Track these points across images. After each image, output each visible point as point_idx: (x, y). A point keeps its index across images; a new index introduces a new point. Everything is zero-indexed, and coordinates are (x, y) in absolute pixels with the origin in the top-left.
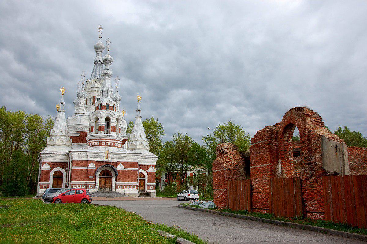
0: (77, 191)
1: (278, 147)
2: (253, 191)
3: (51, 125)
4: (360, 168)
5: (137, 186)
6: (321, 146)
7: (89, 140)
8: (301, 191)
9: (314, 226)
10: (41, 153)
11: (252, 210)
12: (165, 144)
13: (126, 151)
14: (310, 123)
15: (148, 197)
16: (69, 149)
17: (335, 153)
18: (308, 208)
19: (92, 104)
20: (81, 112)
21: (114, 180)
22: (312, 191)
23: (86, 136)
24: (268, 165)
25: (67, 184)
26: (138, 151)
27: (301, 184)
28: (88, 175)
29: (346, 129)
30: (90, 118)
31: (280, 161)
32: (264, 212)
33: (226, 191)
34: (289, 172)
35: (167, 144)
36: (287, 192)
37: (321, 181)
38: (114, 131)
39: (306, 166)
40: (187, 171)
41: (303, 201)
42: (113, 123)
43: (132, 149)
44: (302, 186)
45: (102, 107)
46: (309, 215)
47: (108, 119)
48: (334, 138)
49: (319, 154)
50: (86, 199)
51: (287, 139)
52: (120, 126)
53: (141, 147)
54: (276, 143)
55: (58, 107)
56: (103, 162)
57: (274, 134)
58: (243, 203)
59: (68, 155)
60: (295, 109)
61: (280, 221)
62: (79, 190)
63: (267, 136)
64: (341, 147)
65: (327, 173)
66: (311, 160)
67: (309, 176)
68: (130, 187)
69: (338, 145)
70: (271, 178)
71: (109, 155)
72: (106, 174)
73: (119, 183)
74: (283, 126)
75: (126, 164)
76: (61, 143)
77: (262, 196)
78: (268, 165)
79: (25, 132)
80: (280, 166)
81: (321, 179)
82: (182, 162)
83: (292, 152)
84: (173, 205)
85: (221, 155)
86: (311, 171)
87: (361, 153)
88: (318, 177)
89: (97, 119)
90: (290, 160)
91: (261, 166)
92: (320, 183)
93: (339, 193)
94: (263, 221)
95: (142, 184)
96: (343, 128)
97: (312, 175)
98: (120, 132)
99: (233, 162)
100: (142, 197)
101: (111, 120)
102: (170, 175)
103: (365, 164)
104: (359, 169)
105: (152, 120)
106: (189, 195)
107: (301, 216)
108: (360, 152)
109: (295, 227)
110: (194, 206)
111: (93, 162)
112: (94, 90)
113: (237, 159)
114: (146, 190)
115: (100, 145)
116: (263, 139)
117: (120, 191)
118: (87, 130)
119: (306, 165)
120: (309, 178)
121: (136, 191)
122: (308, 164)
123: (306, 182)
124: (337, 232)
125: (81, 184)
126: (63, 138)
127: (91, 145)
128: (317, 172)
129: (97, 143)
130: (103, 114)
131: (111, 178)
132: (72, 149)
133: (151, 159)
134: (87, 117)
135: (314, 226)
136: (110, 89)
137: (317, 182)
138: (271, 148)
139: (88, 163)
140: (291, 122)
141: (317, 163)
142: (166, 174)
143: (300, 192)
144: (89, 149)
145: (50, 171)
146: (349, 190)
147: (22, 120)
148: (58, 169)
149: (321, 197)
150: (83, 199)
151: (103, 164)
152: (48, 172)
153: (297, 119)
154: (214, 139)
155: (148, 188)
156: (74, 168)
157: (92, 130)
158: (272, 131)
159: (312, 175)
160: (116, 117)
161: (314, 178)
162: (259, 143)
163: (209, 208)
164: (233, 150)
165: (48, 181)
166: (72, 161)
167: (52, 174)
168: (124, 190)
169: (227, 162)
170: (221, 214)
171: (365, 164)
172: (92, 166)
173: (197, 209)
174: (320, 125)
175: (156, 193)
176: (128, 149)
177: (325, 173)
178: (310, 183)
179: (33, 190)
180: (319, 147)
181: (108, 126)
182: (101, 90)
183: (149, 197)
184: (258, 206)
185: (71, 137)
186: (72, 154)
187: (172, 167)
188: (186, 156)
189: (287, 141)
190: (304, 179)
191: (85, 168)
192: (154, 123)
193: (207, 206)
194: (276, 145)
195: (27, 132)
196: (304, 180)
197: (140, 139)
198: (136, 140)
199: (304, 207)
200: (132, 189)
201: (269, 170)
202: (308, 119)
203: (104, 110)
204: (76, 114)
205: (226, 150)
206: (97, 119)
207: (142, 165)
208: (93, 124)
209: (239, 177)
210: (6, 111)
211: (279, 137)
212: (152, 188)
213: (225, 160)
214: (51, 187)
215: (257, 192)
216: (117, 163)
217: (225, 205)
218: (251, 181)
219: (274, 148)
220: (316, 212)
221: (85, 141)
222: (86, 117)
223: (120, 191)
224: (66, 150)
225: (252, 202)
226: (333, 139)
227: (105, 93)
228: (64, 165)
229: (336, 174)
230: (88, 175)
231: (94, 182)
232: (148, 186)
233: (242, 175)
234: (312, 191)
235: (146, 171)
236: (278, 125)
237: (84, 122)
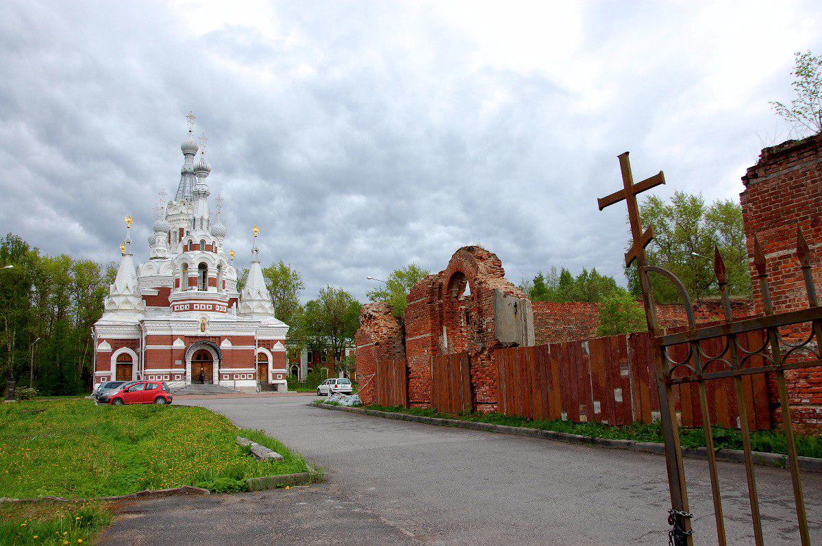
0: (147, 384)
2: (411, 375)
3: (112, 276)
5: (255, 374)
6: (494, 305)
7: (174, 301)
9: (480, 423)
10: (96, 324)
11: (409, 404)
12: (308, 305)
13: (235, 318)
14: (484, 270)
15: (274, 392)
16: (141, 317)
18: (479, 397)
19: (178, 241)
20: (160, 255)
21: (216, 365)
22: (483, 372)
23: (169, 295)
24: (429, 335)
25: (140, 375)
26: (256, 318)
27: (469, 359)
28: (171, 358)
29: (594, 273)
30: (173, 265)
31: (445, 328)
32: (425, 406)
33: (374, 377)
35: (310, 304)
38: (215, 285)
39: (475, 335)
40: (345, 347)
41: (472, 388)
42: (211, 274)
43: (245, 315)
44: (470, 365)
45: (193, 247)
46: (479, 408)
47: (203, 267)
48: (512, 293)
50: (163, 397)
52: (224, 277)
53: (260, 310)
55: (123, 247)
56: (196, 337)
58: (396, 395)
59: (140, 327)
60: (464, 248)
61: (439, 419)
62: (151, 383)
64: (522, 306)
68: (243, 377)
71: (207, 326)
72: (202, 358)
73: (223, 370)
74: (449, 275)
75: (235, 340)
76: (127, 307)
77: (421, 383)
78: (429, 335)
79: (72, 290)
82: (335, 333)
84: (302, 403)
87: (585, 311)
88: (491, 351)
89: (186, 266)
90: (462, 327)
91: (419, 337)
93: (514, 372)
94: (419, 421)
95: (264, 372)
96: (589, 272)
97: (484, 349)
98: (224, 288)
99: (385, 332)
100: (263, 393)
101: (209, 267)
102: (316, 357)
105: (282, 266)
106: (336, 386)
107: (469, 409)
109: (457, 425)
110: (332, 403)
111: (180, 336)
112: (182, 218)
113: (392, 328)
114: (271, 380)
115: (191, 309)
116: (421, 296)
117: (227, 383)
118: (170, 284)
120: (480, 353)
121: (253, 383)
122: (479, 332)
125: (163, 375)
126: (131, 299)
127: (176, 309)
129: (208, 306)
130: (195, 257)
131: (212, 362)
132: (145, 316)
133: (277, 330)
134: (170, 263)
135: (480, 423)
136: (206, 217)
137: (489, 357)
138: (432, 310)
139: (172, 339)
142: (309, 355)
144: (173, 317)
145: (112, 354)
147: (66, 270)
148: (125, 350)
150: (156, 400)
151: (197, 340)
152: (107, 356)
153: (467, 266)
154: (385, 295)
155: (275, 377)
156: (149, 347)
157: (177, 285)
158: (434, 283)
160: (217, 263)
161: (486, 353)
164: (386, 313)
165: (109, 368)
166: (147, 337)
167: (114, 358)
168: (232, 381)
169: (375, 332)
170: (366, 414)
172: (179, 344)
173: (334, 407)
175: (286, 384)
176: (239, 314)
177: (499, 345)
179: (88, 387)
181: (204, 277)
182: (191, 218)
183: (276, 392)
184: (416, 399)
185: (144, 297)
186: (146, 325)
187: (320, 342)
188: (340, 323)
189: (457, 298)
190: (473, 355)
191: (168, 347)
192: (284, 271)
193: (350, 403)
194: (440, 305)
195: (76, 291)
197: (259, 298)
198: (252, 300)
199: (474, 395)
200: (247, 379)
201: (430, 344)
202: (481, 265)
203: (197, 252)
204: (151, 259)
205: (374, 314)
206: (186, 266)
207: (263, 341)
208: (179, 276)
210: (41, 255)
211: (444, 292)
212: (279, 377)
213: (372, 330)
214: (113, 379)
215: (415, 378)
216: (220, 339)
217: (373, 400)
218: (406, 361)
219: (437, 309)
220: (487, 403)
221: (168, 304)
222: (167, 263)
223: (227, 383)
224: (136, 318)
225: (408, 393)
227: (198, 223)
228: (133, 344)
229: (515, 345)
230: (171, 358)
231: (184, 370)
232: (273, 374)
234: (483, 372)
235: (270, 350)
236: (443, 274)
237: (165, 272)
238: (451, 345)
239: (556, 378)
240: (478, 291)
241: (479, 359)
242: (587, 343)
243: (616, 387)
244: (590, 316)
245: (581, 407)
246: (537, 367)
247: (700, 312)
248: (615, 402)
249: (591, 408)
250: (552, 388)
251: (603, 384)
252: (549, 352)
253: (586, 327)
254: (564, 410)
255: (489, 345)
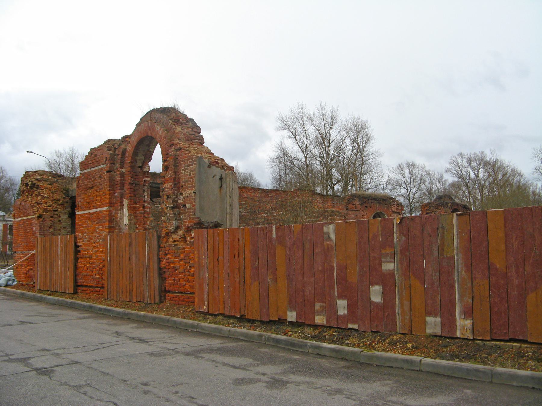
1: (124, 177)
2: (79, 256)
4: (251, 218)
8: (158, 255)
17: (219, 190)
24: (106, 208)
31: (126, 202)
34: (141, 222)
36: (134, 257)
37: (193, 238)
49: (192, 190)
51: (141, 165)
54: (121, 171)
57: (118, 155)
63: (106, 157)
65: (203, 225)
66: (177, 201)
67: (172, 228)
69: (224, 176)
70: (109, 232)
74: (134, 140)
78: (106, 208)
80: (126, 211)
81: (193, 235)
83: (148, 188)
85: (29, 191)
86: (176, 219)
87: (254, 196)
88: (188, 230)
90: (144, 201)
91: (94, 210)
92: (190, 242)
93: (221, 258)
97: (178, 228)
103: (259, 212)
104: (250, 220)
108: (253, 194)
116: (98, 163)
119: (168, 208)
120: (172, 233)
123: (167, 241)
124: (212, 328)
128: (186, 222)
137: (185, 239)
138: (111, 179)
140: (150, 134)
141: (188, 206)
143: (155, 258)
146: (237, 254)
147: (464, 318)
149: (190, 267)
159: (178, 228)
161: (180, 232)
162: (93, 169)
163: (7, 285)
171: (259, 212)
174: (197, 140)
178: (175, 241)
180: (191, 178)
189: (141, 167)
196: (164, 237)
201: (107, 219)
205: (37, 183)
209: (60, 230)
219: (118, 178)
226: (217, 165)
233: (65, 228)
238: (132, 222)
239: (281, 270)
240: (176, 159)
241: (171, 239)
242: (332, 227)
243: (373, 284)
244: (259, 201)
245: (318, 306)
246: (255, 253)
247: (353, 204)
248: (371, 302)
249: (333, 308)
250: (275, 280)
251: (353, 279)
252: (274, 236)
253: (255, 212)
254: (292, 309)
255: (186, 224)
